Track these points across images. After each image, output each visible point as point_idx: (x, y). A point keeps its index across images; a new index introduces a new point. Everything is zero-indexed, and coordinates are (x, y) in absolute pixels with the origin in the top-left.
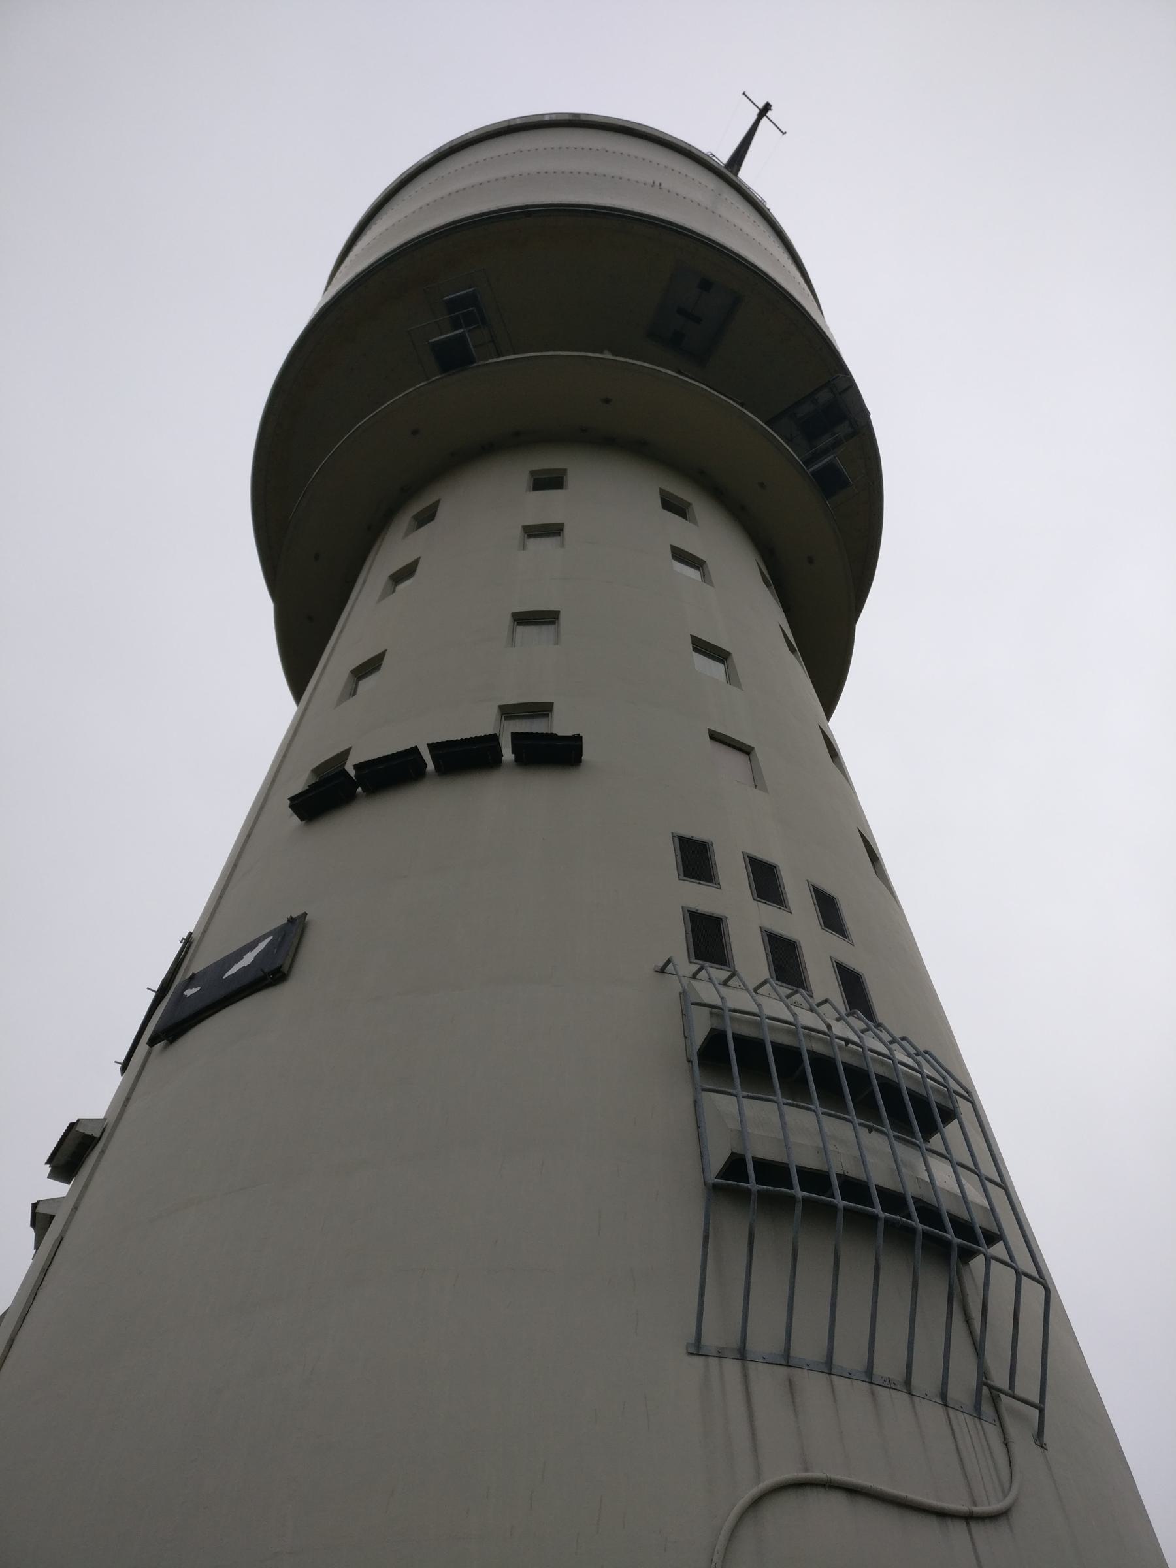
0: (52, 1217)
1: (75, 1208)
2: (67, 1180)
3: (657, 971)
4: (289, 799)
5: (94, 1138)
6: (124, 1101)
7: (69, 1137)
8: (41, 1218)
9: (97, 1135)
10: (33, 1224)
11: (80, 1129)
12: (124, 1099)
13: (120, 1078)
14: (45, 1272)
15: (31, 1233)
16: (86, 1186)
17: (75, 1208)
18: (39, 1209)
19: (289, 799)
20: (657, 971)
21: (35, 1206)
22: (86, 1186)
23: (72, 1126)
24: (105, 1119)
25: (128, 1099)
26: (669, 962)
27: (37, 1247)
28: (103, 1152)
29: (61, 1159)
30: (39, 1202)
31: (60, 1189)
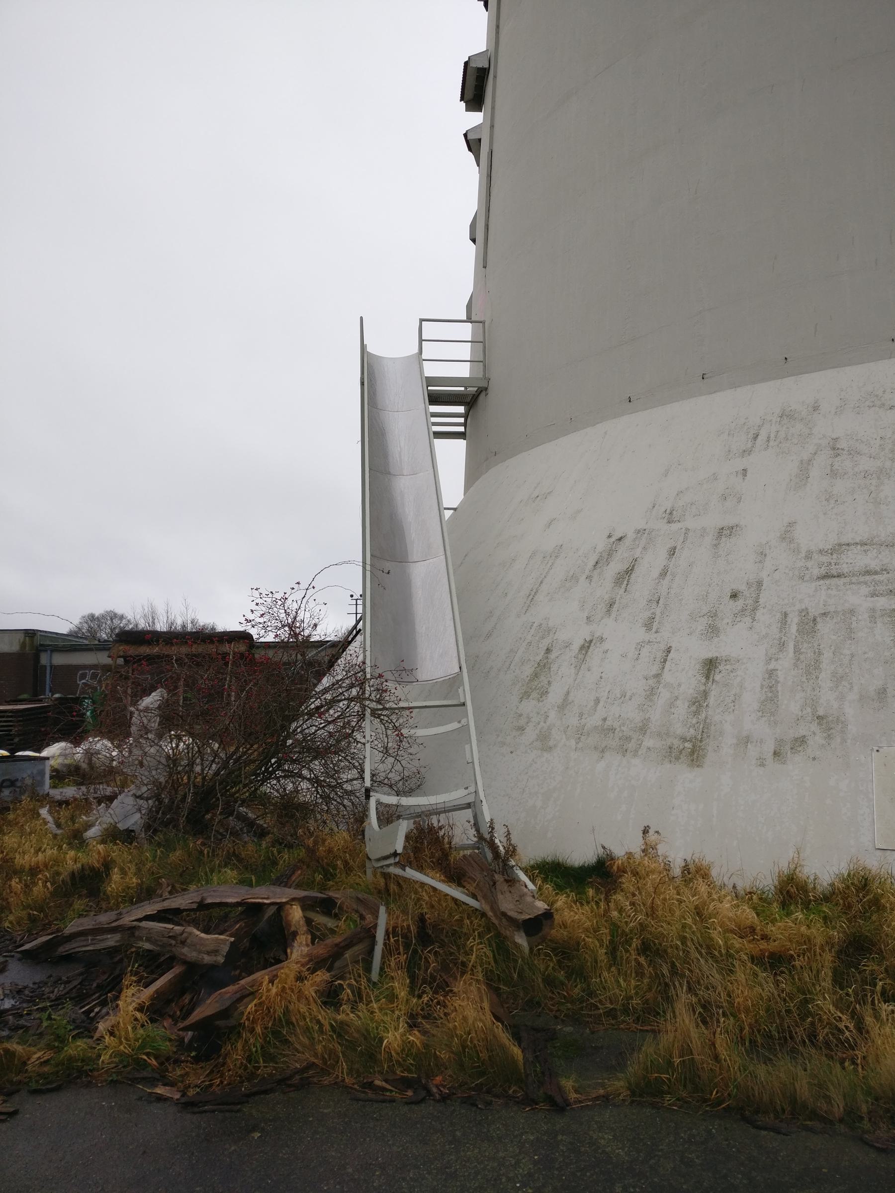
0: (480, 140)
1: (492, 126)
2: (479, 110)
3: (568, 693)
4: (461, 101)
5: (486, 69)
6: (496, 29)
7: (466, 92)
8: (473, 144)
9: (486, 66)
10: (470, 149)
11: (473, 65)
12: (495, 27)
13: (485, 14)
14: (490, 176)
15: (471, 156)
16: (493, 108)
17: (492, 126)
18: (469, 137)
19: (461, 101)
20: (568, 693)
21: (465, 135)
22: (493, 108)
23: (466, 64)
24: (487, 50)
25: (498, 27)
26: (645, 831)
27: (478, 165)
28: (495, 77)
29: (469, 95)
30: (467, 131)
31: (477, 118)
